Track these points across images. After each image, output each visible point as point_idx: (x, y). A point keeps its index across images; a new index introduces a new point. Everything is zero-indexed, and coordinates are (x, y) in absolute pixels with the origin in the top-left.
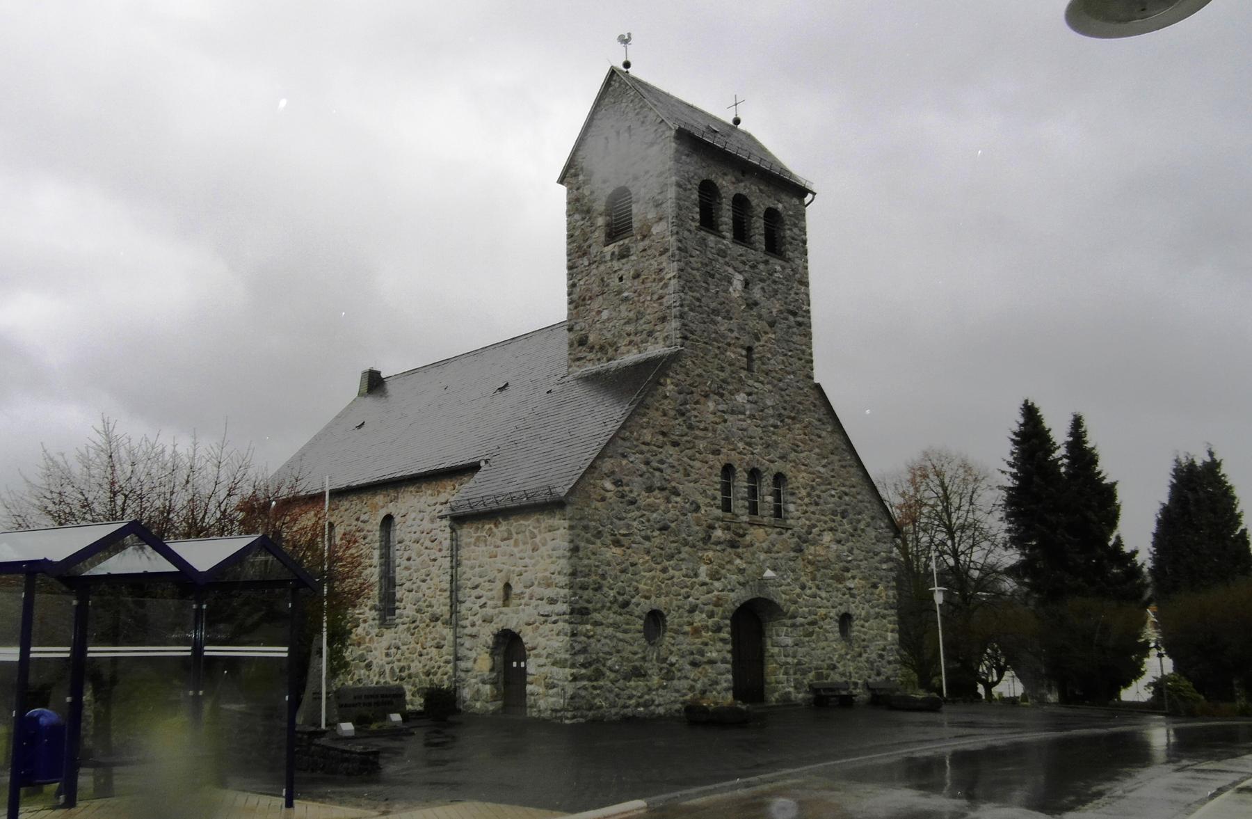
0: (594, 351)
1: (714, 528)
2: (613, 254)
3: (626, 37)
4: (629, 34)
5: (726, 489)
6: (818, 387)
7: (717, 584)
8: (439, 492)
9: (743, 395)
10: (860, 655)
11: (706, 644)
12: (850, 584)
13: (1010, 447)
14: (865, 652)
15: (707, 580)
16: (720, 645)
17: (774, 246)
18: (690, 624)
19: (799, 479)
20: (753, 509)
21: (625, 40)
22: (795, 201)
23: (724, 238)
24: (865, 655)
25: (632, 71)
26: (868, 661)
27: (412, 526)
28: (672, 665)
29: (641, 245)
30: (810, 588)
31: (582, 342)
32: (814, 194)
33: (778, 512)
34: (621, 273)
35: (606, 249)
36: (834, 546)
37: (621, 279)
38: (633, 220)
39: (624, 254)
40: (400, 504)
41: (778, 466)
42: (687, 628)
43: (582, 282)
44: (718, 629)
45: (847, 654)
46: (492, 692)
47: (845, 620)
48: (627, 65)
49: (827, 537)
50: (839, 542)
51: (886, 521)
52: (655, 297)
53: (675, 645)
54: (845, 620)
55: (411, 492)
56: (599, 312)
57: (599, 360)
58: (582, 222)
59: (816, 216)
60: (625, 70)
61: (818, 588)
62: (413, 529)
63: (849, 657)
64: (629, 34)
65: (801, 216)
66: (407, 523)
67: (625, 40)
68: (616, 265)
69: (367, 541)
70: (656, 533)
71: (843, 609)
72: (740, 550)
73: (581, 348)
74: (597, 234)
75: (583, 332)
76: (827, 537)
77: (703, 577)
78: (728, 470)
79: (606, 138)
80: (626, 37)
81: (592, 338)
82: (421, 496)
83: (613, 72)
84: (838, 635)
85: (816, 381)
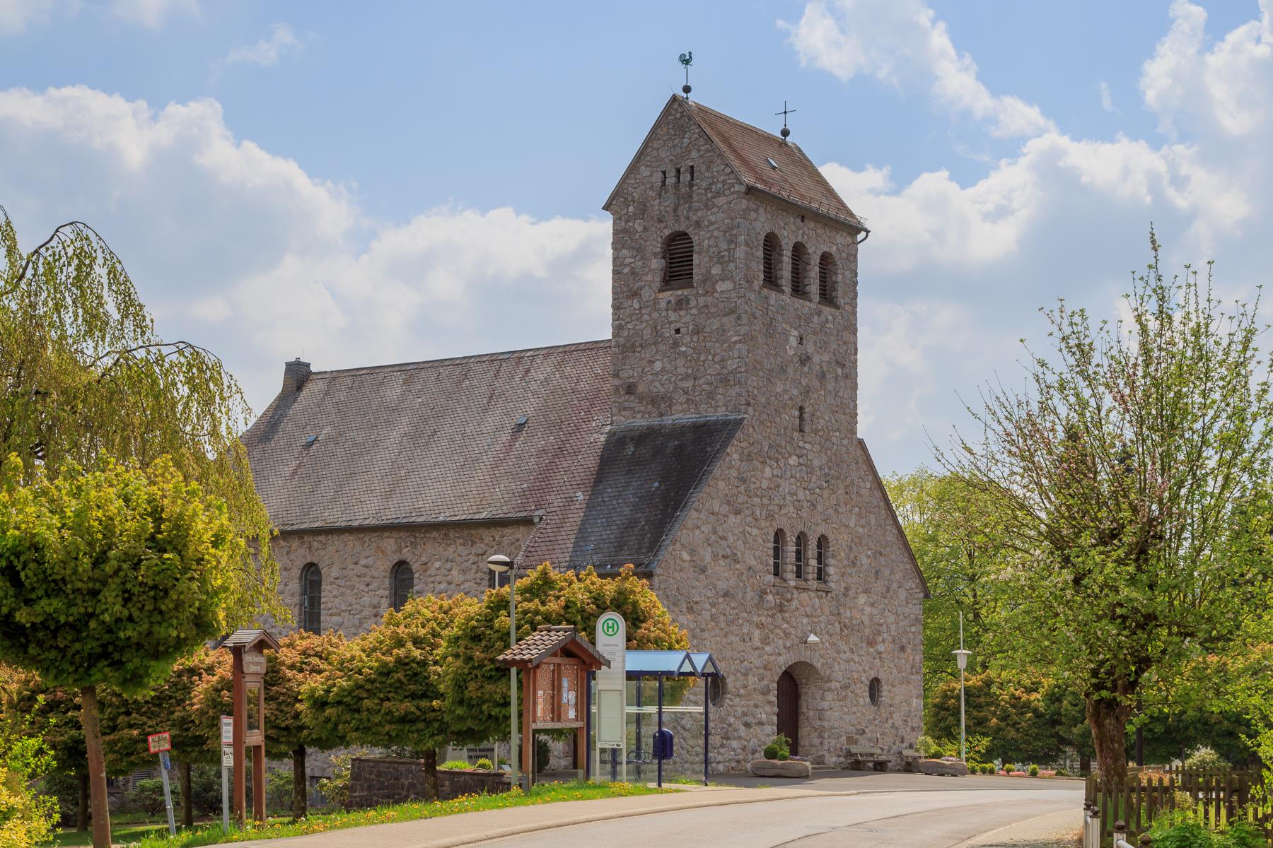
0: (644, 403)
1: (766, 593)
2: (669, 302)
3: (687, 57)
4: (690, 53)
5: (777, 552)
6: (861, 443)
7: (767, 648)
8: (473, 543)
9: (794, 457)
10: (887, 721)
11: (756, 706)
12: (881, 648)
13: (1083, 144)
14: (892, 718)
15: (760, 645)
16: (768, 708)
17: (827, 297)
18: (745, 687)
19: (840, 541)
20: (799, 574)
21: (686, 61)
22: (849, 240)
23: (783, 292)
24: (890, 721)
25: (693, 98)
26: (893, 726)
27: (435, 575)
28: (730, 725)
29: (702, 300)
30: (845, 653)
31: (630, 389)
32: (868, 232)
33: (821, 575)
34: (678, 325)
35: (661, 295)
36: (868, 609)
37: (678, 331)
38: (694, 271)
39: (680, 304)
40: (419, 550)
41: (821, 530)
42: (742, 691)
43: (629, 326)
44: (765, 692)
45: (875, 719)
46: (564, 748)
47: (874, 687)
48: (687, 89)
49: (862, 599)
50: (872, 605)
51: (917, 581)
52: (717, 358)
53: (734, 705)
54: (874, 687)
55: (435, 539)
56: (651, 362)
57: (649, 413)
58: (632, 260)
59: (866, 253)
60: (685, 95)
61: (852, 651)
62: (438, 578)
63: (876, 722)
64: (690, 53)
65: (853, 258)
66: (429, 572)
67: (686, 61)
68: (673, 316)
69: (371, 587)
70: (721, 600)
71: (873, 674)
72: (787, 615)
73: (627, 397)
74: (650, 277)
75: (631, 380)
76: (862, 599)
77: (757, 642)
78: (779, 535)
79: (664, 173)
80: (687, 57)
81: (641, 388)
82: (448, 545)
83: (674, 98)
84: (868, 700)
85: (859, 436)
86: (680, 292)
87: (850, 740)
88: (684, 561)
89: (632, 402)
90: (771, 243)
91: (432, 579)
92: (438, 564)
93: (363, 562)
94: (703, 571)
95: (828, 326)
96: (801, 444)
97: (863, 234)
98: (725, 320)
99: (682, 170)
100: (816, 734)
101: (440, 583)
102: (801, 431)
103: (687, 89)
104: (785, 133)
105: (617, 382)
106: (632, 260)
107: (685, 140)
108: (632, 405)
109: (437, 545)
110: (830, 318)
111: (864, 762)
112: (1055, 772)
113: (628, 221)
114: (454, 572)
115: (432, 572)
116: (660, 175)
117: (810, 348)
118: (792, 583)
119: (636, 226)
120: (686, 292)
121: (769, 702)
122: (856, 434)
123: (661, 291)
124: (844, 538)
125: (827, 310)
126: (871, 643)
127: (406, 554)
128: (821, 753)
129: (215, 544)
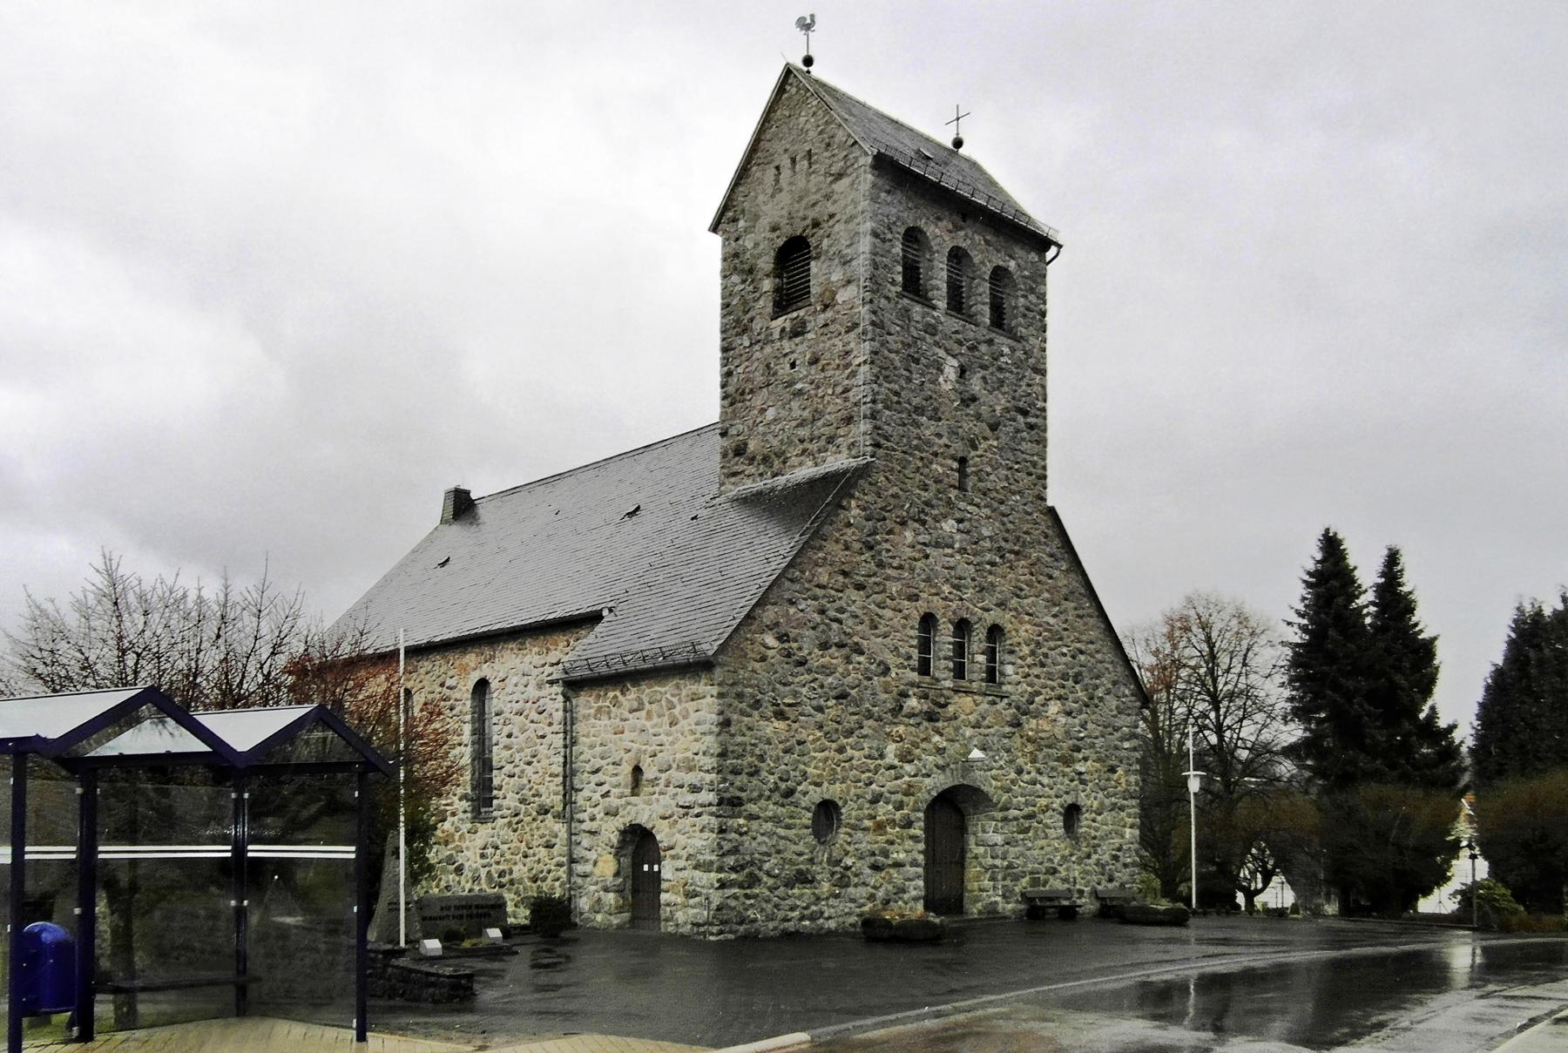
2: (783, 330)
3: (808, 21)
4: (812, 16)
5: (925, 646)
6: (1052, 512)
7: (908, 768)
10: (1089, 856)
11: (892, 843)
14: (1096, 852)
15: (896, 762)
16: (909, 844)
18: (872, 817)
19: (1020, 633)
20: (959, 672)
21: (806, 25)
22: (1034, 257)
24: (1095, 857)
29: (822, 318)
32: (1060, 246)
33: (991, 675)
35: (774, 324)
36: (1062, 720)
37: (793, 365)
39: (798, 331)
40: (497, 665)
41: (993, 616)
42: (868, 823)
43: (740, 370)
45: (1071, 855)
46: (617, 901)
47: (1072, 813)
48: (808, 61)
50: (1069, 714)
52: (839, 389)
54: (1072, 813)
55: (512, 649)
56: (763, 411)
58: (742, 287)
59: (1058, 275)
60: (805, 69)
62: (515, 697)
64: (812, 16)
67: (806, 25)
68: (787, 345)
69: (454, 712)
70: (832, 702)
71: (1069, 799)
72: (940, 724)
73: (737, 458)
75: (741, 438)
76: (1054, 708)
77: (891, 758)
78: (928, 621)
79: (777, 168)
80: (808, 21)
83: (788, 72)
84: (1061, 831)
85: (1050, 503)
87: (1035, 882)
88: (769, 648)
89: (739, 465)
91: (510, 698)
96: (962, 505)
97: (1053, 250)
98: (847, 338)
99: (798, 158)
100: (988, 876)
101: (517, 702)
102: (961, 487)
103: (808, 61)
104: (958, 143)
105: (726, 442)
107: (801, 119)
108: (742, 468)
109: (514, 656)
110: (1006, 350)
111: (1043, 908)
114: (530, 688)
116: (774, 171)
118: (948, 684)
119: (746, 244)
122: (1045, 500)
125: (1004, 344)
127: (486, 671)
128: (993, 899)
129: (497, 715)
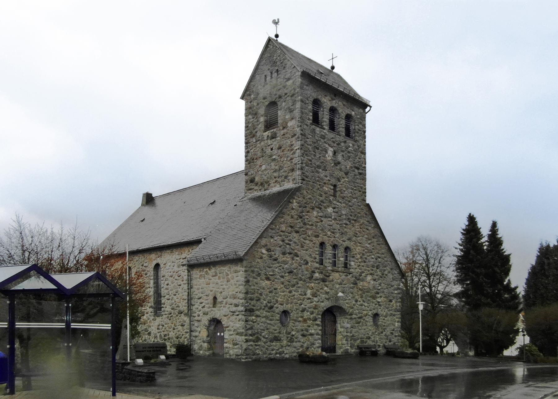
0: (258, 185)
1: (314, 272)
3: (277, 21)
4: (278, 19)
6: (368, 205)
7: (315, 299)
8: (182, 253)
9: (331, 209)
10: (382, 333)
11: (309, 326)
12: (379, 300)
15: (311, 297)
21: (276, 23)
22: (361, 110)
24: (384, 333)
25: (280, 40)
26: (385, 335)
27: (169, 269)
28: (293, 335)
29: (282, 132)
30: (360, 302)
31: (252, 181)
32: (371, 107)
36: (372, 282)
37: (272, 149)
38: (278, 119)
39: (273, 137)
43: (252, 151)
45: (376, 332)
46: (208, 346)
48: (277, 36)
49: (369, 278)
50: (375, 280)
52: (289, 159)
55: (168, 253)
56: (261, 166)
58: (253, 120)
60: (276, 39)
64: (278, 19)
66: (166, 268)
67: (276, 23)
68: (269, 142)
69: (147, 276)
70: (287, 274)
72: (327, 283)
73: (251, 184)
75: (253, 176)
78: (322, 244)
80: (277, 21)
81: (257, 179)
83: (269, 40)
85: (367, 202)
86: (272, 130)
89: (252, 186)
90: (316, 102)
91: (167, 271)
92: (169, 264)
93: (144, 265)
94: (276, 260)
95: (350, 149)
105: (247, 178)
106: (253, 120)
109: (169, 255)
112: (324, 127)
113: (251, 102)
115: (167, 267)
117: (340, 158)
120: (275, 130)
121: (317, 325)
123: (265, 132)
124: (358, 249)
126: (374, 297)
127: (159, 261)
